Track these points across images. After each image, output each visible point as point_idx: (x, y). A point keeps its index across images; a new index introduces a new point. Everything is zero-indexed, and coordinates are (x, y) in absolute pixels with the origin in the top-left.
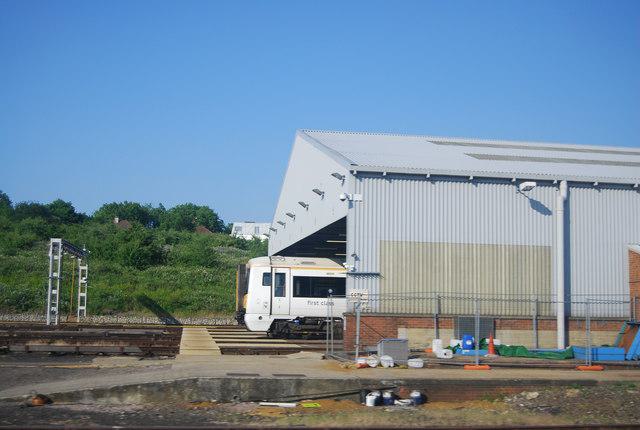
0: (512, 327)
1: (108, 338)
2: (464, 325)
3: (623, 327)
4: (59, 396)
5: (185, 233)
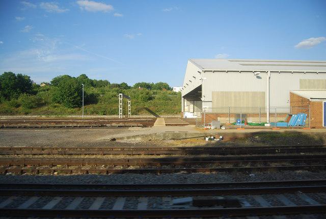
0: (253, 116)
1: (135, 121)
2: (238, 116)
3: (287, 116)
4: (118, 138)
5: (159, 91)
